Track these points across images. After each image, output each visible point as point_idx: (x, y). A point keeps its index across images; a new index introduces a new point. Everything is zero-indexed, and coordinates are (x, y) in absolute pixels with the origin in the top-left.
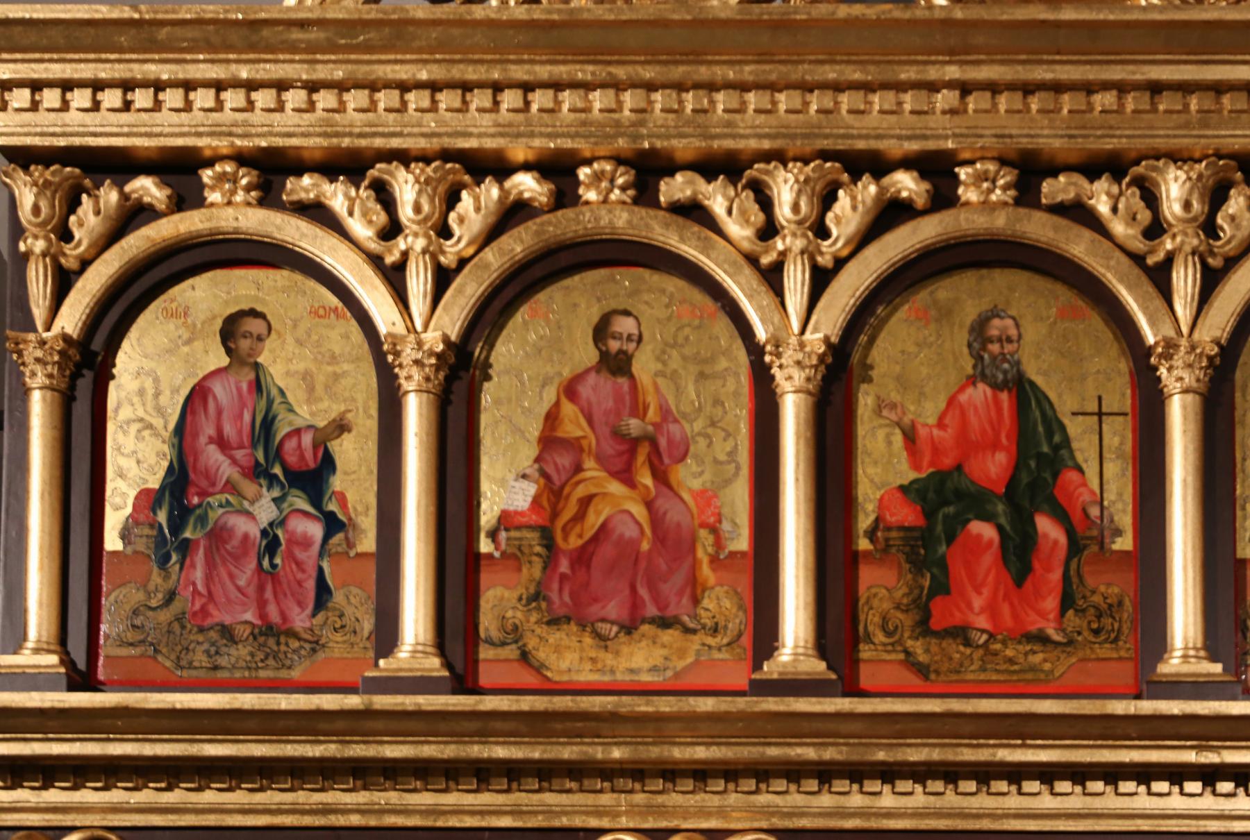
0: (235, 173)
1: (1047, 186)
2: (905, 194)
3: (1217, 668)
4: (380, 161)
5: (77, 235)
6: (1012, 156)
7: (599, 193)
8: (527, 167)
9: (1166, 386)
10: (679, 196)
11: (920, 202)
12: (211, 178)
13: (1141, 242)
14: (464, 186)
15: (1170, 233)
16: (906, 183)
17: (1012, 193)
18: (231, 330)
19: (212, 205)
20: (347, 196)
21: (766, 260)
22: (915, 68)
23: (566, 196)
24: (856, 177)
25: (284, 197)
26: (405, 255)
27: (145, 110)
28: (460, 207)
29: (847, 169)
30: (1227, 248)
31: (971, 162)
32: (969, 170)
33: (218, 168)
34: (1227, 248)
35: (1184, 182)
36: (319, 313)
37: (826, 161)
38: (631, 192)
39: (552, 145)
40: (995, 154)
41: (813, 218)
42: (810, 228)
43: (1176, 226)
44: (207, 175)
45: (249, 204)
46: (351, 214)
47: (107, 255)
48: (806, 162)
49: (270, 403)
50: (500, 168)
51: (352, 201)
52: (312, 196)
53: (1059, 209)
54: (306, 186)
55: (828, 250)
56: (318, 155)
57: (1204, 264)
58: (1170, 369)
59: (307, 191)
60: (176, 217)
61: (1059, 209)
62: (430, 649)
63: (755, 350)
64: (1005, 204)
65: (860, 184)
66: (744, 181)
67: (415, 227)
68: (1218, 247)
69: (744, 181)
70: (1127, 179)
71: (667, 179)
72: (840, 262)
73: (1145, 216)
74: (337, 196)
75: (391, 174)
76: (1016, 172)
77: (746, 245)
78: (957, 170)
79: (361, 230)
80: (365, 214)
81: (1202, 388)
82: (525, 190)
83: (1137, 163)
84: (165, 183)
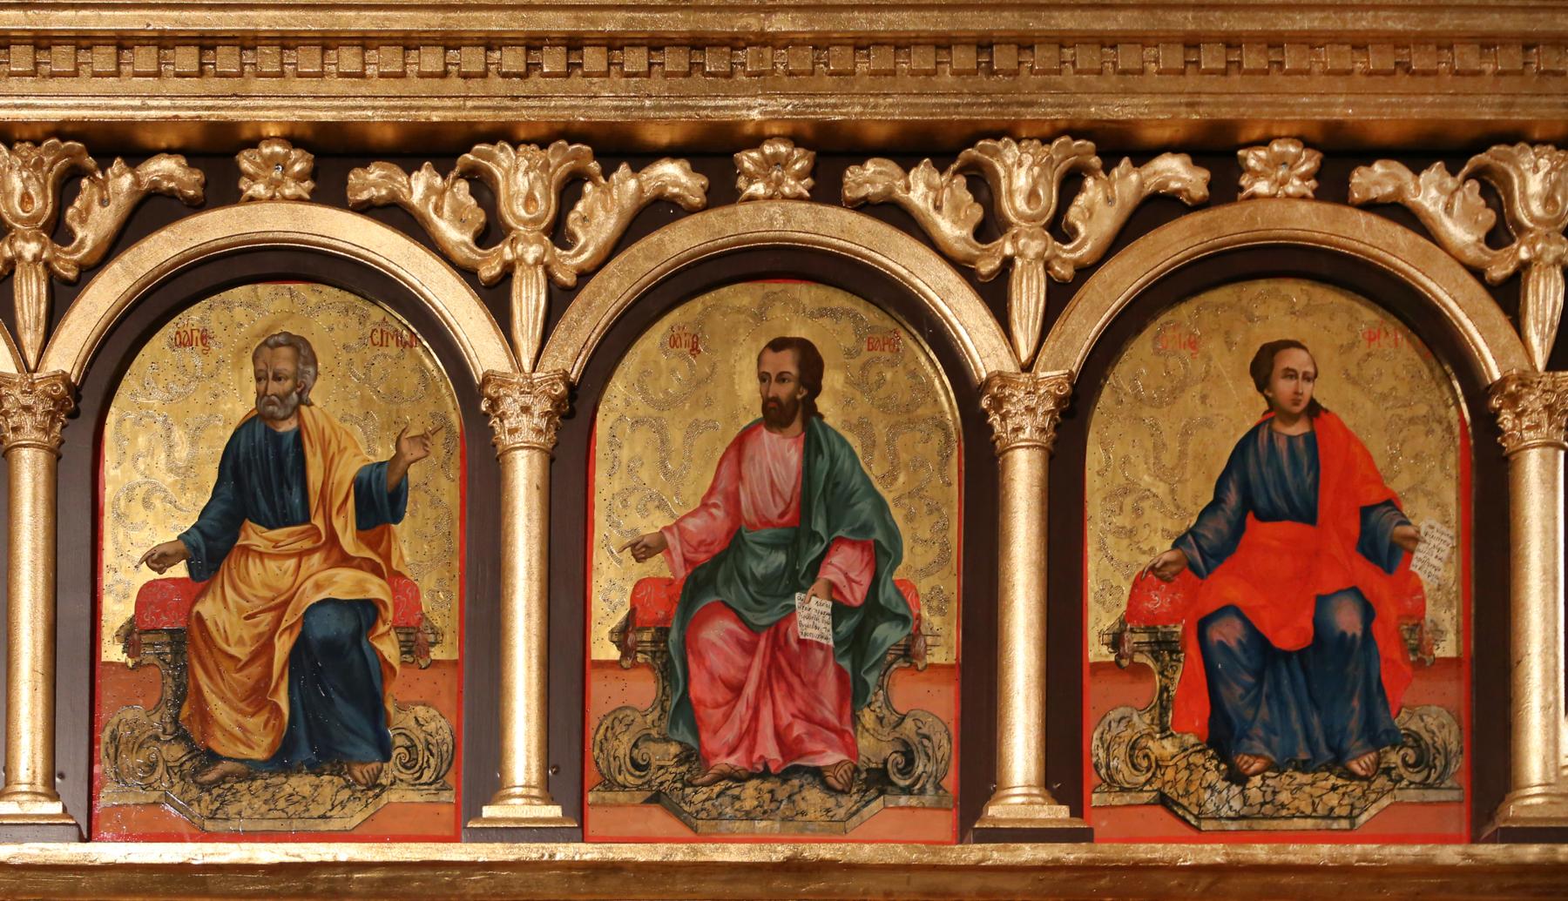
0: (287, 156)
1: (853, 175)
2: (1174, 185)
3: (555, 811)
4: (481, 142)
5: (80, 234)
6: (808, 132)
7: (768, 185)
8: (170, 151)
9: (999, 438)
10: (869, 189)
11: (697, 199)
12: (754, 162)
13: (972, 246)
14: (1091, 171)
15: (1009, 235)
16: (1175, 171)
17: (1312, 183)
18: (1263, 368)
19: (252, 199)
20: (929, 186)
21: (1497, 272)
22: (1317, 14)
23: (1225, 188)
24: (104, 161)
25: (847, 194)
26: (1008, 262)
27: (557, 75)
28: (1081, 200)
29: (597, 156)
30: (1078, 254)
31: (1264, 142)
32: (1262, 154)
33: (768, 149)
34: (1078, 254)
35: (1549, 173)
36: (381, 337)
37: (1075, 138)
38: (308, 184)
39: (1195, 117)
40: (1295, 130)
41: (49, 211)
42: (44, 228)
43: (1531, 231)
44: (748, 160)
45: (300, 199)
46: (438, 209)
47: (115, 267)
48: (1046, 140)
49: (833, 460)
50: (642, 156)
51: (937, 190)
52: (384, 192)
53: (865, 206)
54: (372, 180)
55: (569, 264)
56: (389, 135)
57: (550, 278)
58: (1004, 418)
59: (872, 183)
60: (713, 216)
61: (1370, 206)
62: (535, 792)
63: (1478, 392)
64: (1304, 197)
65: (1116, 172)
66: (457, 169)
67: (1541, 229)
68: (1065, 251)
69: (457, 169)
70: (954, 167)
71: (1363, 169)
72: (1084, 272)
73: (1488, 217)
74: (419, 186)
75: (490, 157)
76: (812, 154)
77: (1472, 254)
78: (1240, 153)
79: (952, 229)
80: (956, 208)
81: (1042, 439)
82: (1171, 179)
83: (971, 143)
84: (696, 169)
